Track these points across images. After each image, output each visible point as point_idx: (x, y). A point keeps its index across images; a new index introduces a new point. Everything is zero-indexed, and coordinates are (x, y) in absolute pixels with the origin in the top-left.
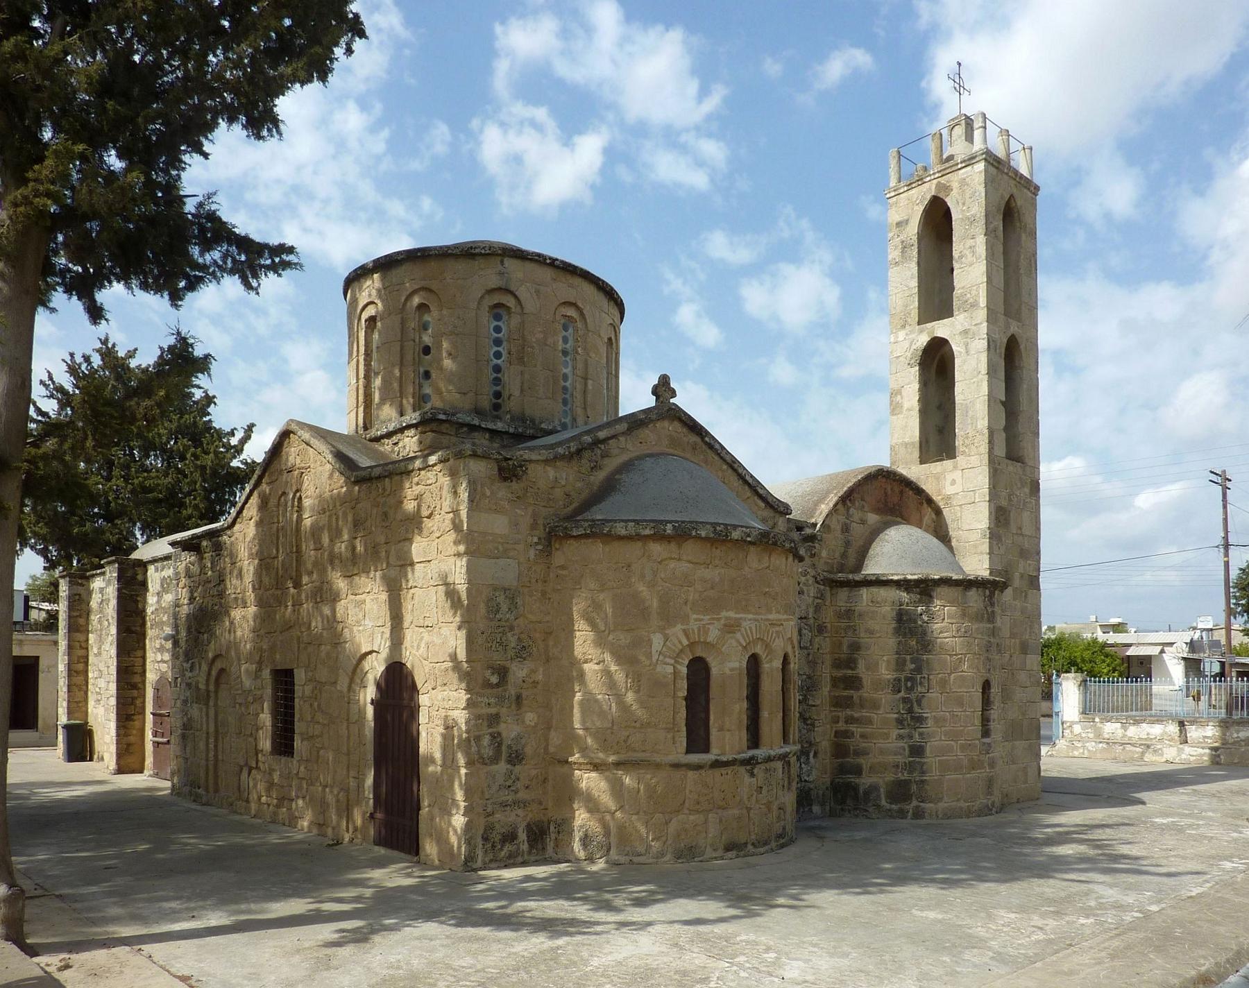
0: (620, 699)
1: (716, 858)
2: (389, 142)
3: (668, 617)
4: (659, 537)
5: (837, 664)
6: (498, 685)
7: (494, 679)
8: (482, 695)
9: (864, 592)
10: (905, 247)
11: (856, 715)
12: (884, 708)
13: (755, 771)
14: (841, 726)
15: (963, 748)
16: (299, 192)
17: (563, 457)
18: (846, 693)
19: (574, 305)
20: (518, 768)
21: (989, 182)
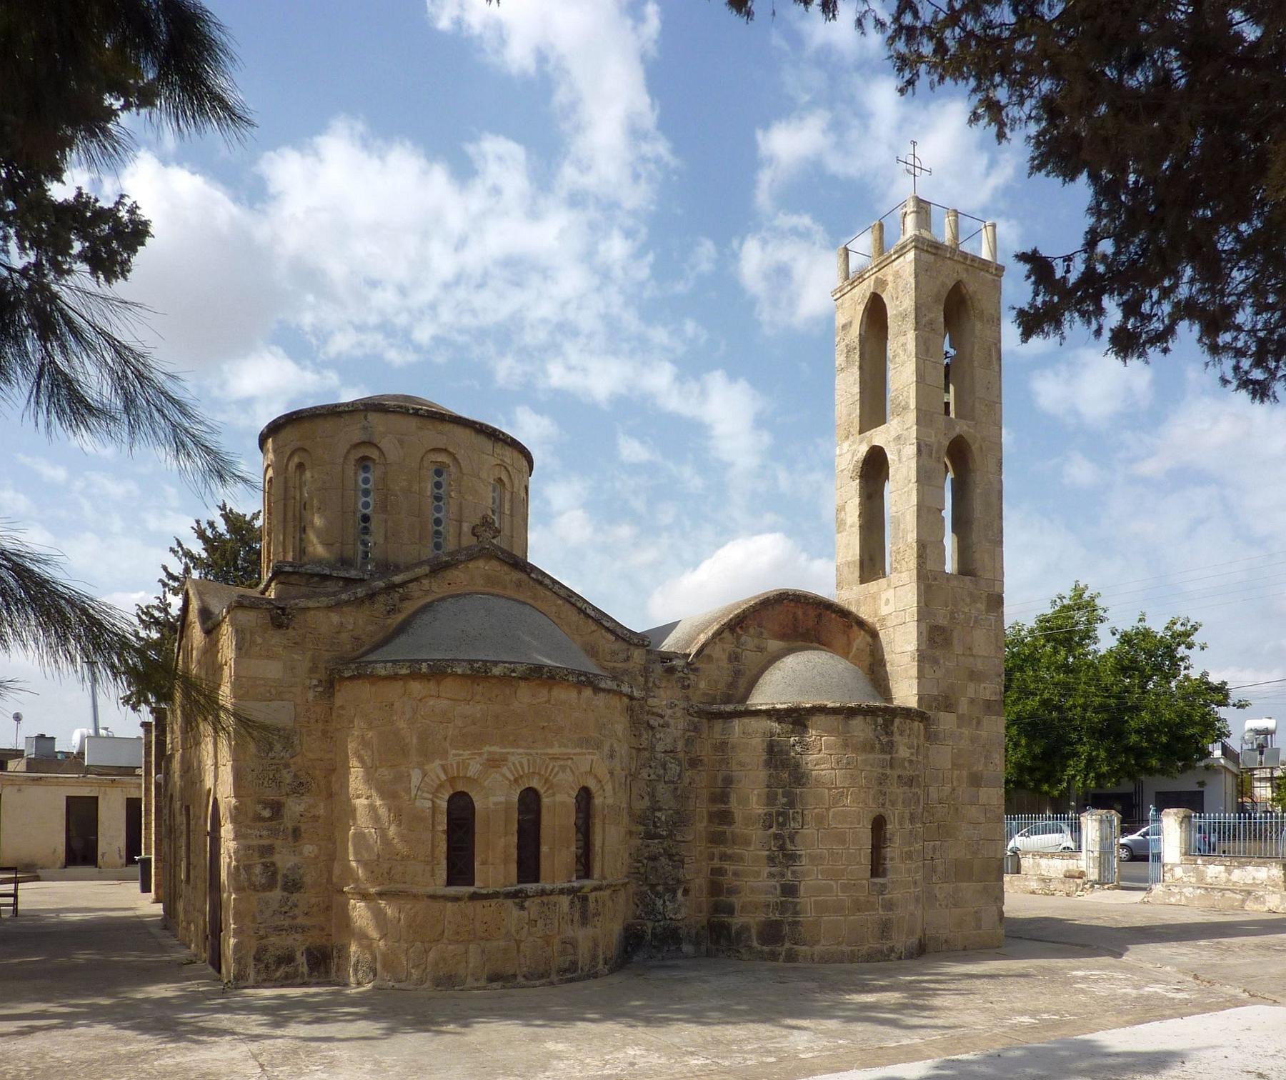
0: (383, 832)
1: (478, 988)
2: (654, 267)
3: (426, 755)
4: (415, 675)
5: (714, 799)
6: (271, 819)
7: (267, 813)
9: (736, 722)
10: (849, 351)
11: (729, 852)
12: (754, 845)
13: (526, 904)
14: (716, 863)
15: (845, 888)
16: (565, 329)
17: (347, 602)
18: (720, 828)
20: (295, 897)
21: (921, 270)
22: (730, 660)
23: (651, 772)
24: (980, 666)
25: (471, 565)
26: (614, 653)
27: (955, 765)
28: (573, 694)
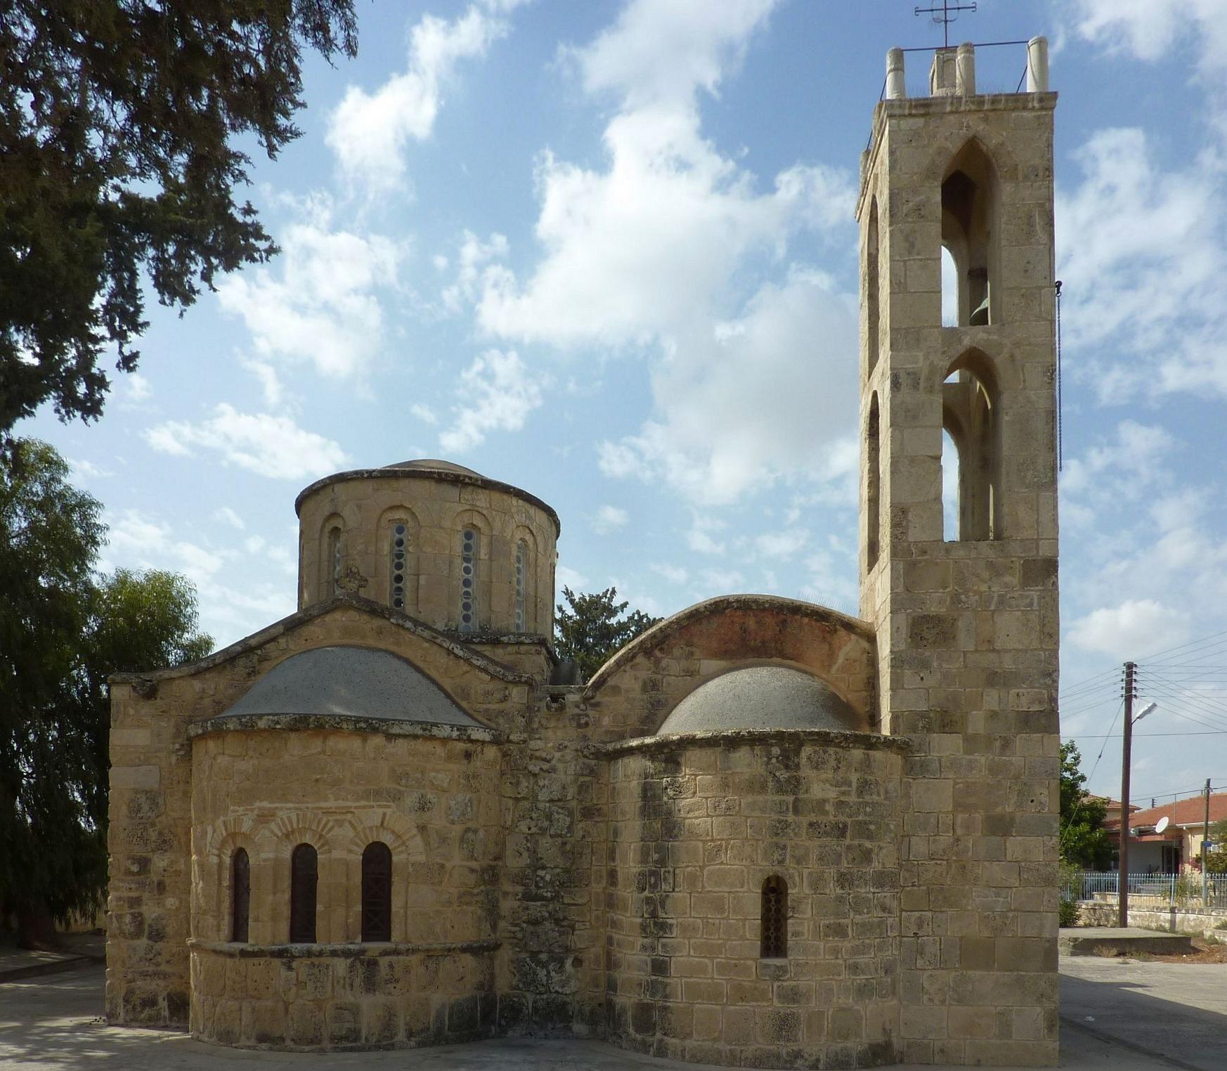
6: (139, 873)
7: (135, 868)
8: (122, 881)
13: (294, 965)
15: (722, 968)
19: (401, 507)
22: (644, 689)
23: (533, 824)
24: (1008, 663)
25: (328, 618)
26: (487, 693)
27: (959, 806)
28: (356, 743)
